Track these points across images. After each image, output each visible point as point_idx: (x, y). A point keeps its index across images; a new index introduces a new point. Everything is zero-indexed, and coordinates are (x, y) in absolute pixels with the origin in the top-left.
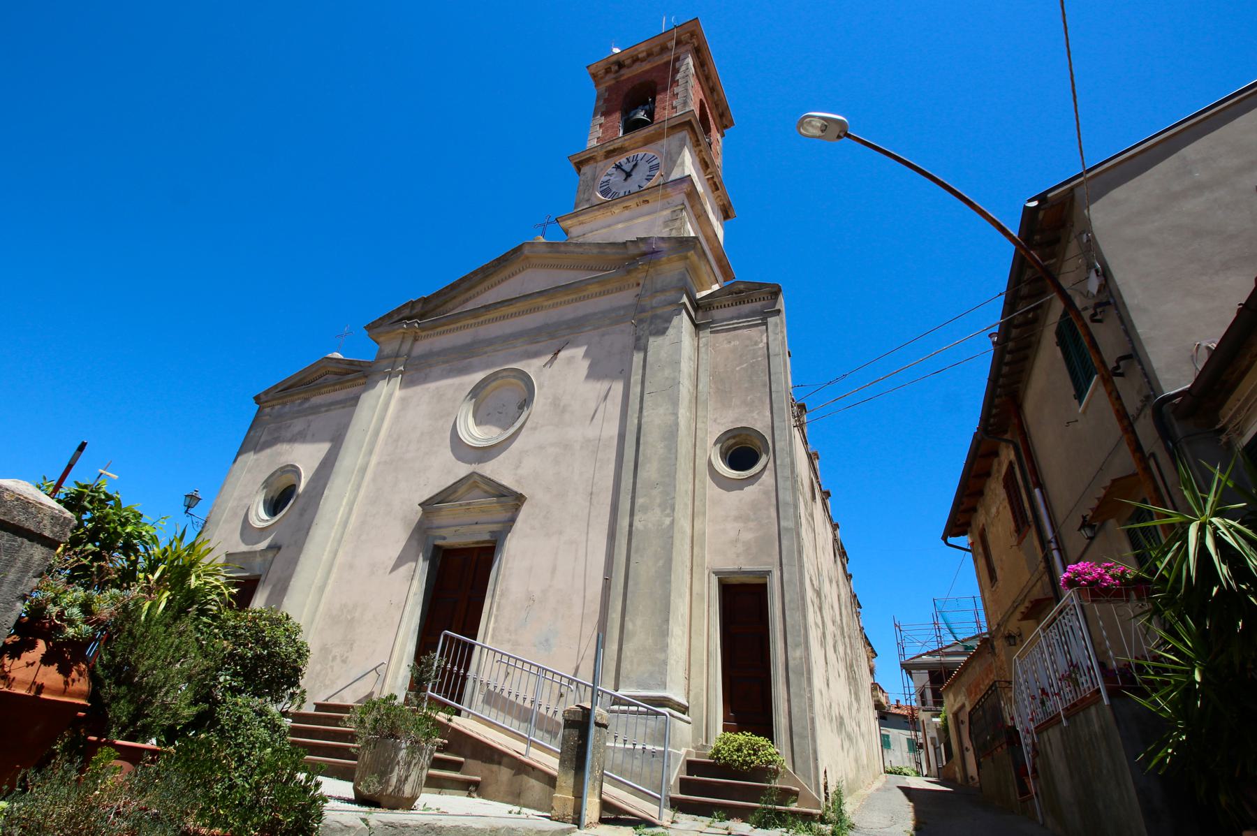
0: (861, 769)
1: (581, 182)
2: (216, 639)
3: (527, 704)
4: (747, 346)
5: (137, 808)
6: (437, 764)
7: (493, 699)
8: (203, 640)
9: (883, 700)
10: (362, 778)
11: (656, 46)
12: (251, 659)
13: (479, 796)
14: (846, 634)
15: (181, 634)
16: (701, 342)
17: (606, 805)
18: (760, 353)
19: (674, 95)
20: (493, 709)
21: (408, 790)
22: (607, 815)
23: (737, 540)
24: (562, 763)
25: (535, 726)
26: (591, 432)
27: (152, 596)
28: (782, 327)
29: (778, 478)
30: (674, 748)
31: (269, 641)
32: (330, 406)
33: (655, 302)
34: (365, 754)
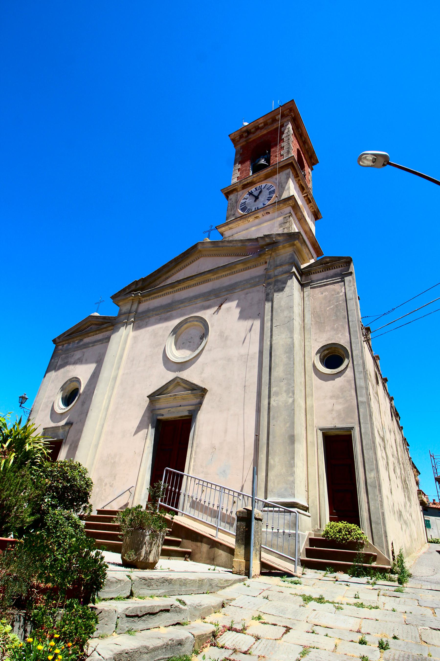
0: (413, 541)
1: (229, 204)
2: (42, 478)
3: (215, 508)
4: (333, 295)
5: (5, 575)
6: (167, 542)
7: (195, 505)
8: (35, 479)
9: (425, 500)
10: (126, 552)
11: (269, 119)
12: (61, 489)
13: (191, 560)
14: (401, 463)
15: (23, 476)
16: (305, 294)
17: (263, 565)
18: (341, 298)
19: (281, 148)
20: (196, 511)
21: (151, 559)
22: (264, 571)
23: (332, 410)
24: (237, 541)
25: (220, 520)
26: (243, 351)
27: (6, 456)
28: (354, 282)
29: (356, 372)
30: (301, 531)
31: (70, 479)
32: (94, 343)
33: (276, 272)
34: (126, 539)
